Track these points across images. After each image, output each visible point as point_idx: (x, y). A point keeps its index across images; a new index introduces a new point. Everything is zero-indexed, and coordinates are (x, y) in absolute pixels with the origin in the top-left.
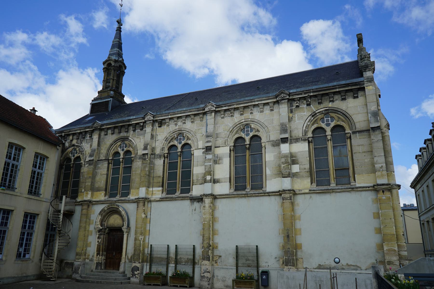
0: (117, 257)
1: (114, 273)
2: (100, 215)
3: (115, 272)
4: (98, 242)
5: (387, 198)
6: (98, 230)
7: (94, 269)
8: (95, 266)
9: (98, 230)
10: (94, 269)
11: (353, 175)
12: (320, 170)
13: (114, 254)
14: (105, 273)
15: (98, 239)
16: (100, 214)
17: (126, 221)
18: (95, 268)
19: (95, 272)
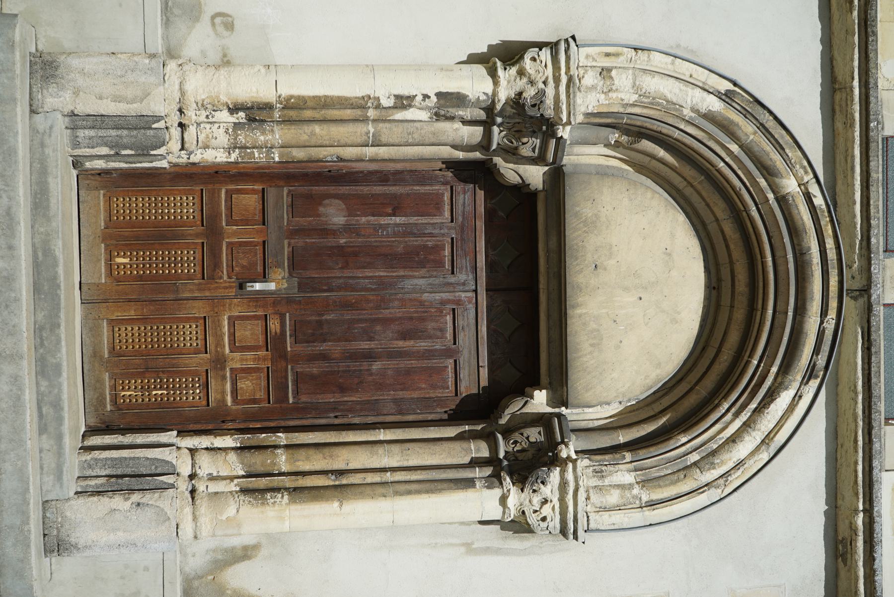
0: (232, 321)
1: (42, 430)
2: (718, 95)
3: (59, 438)
4: (403, 102)
5: (542, 115)
6: (542, 94)
7: (76, 93)
8: (110, 108)
9: (550, 91)
10: (76, 93)
11: (765, 297)
12: (837, 220)
13: (258, 286)
14: (37, 289)
15: (439, 95)
16: (727, 97)
17: (652, 504)
18: (88, 106)
19: (34, 130)
